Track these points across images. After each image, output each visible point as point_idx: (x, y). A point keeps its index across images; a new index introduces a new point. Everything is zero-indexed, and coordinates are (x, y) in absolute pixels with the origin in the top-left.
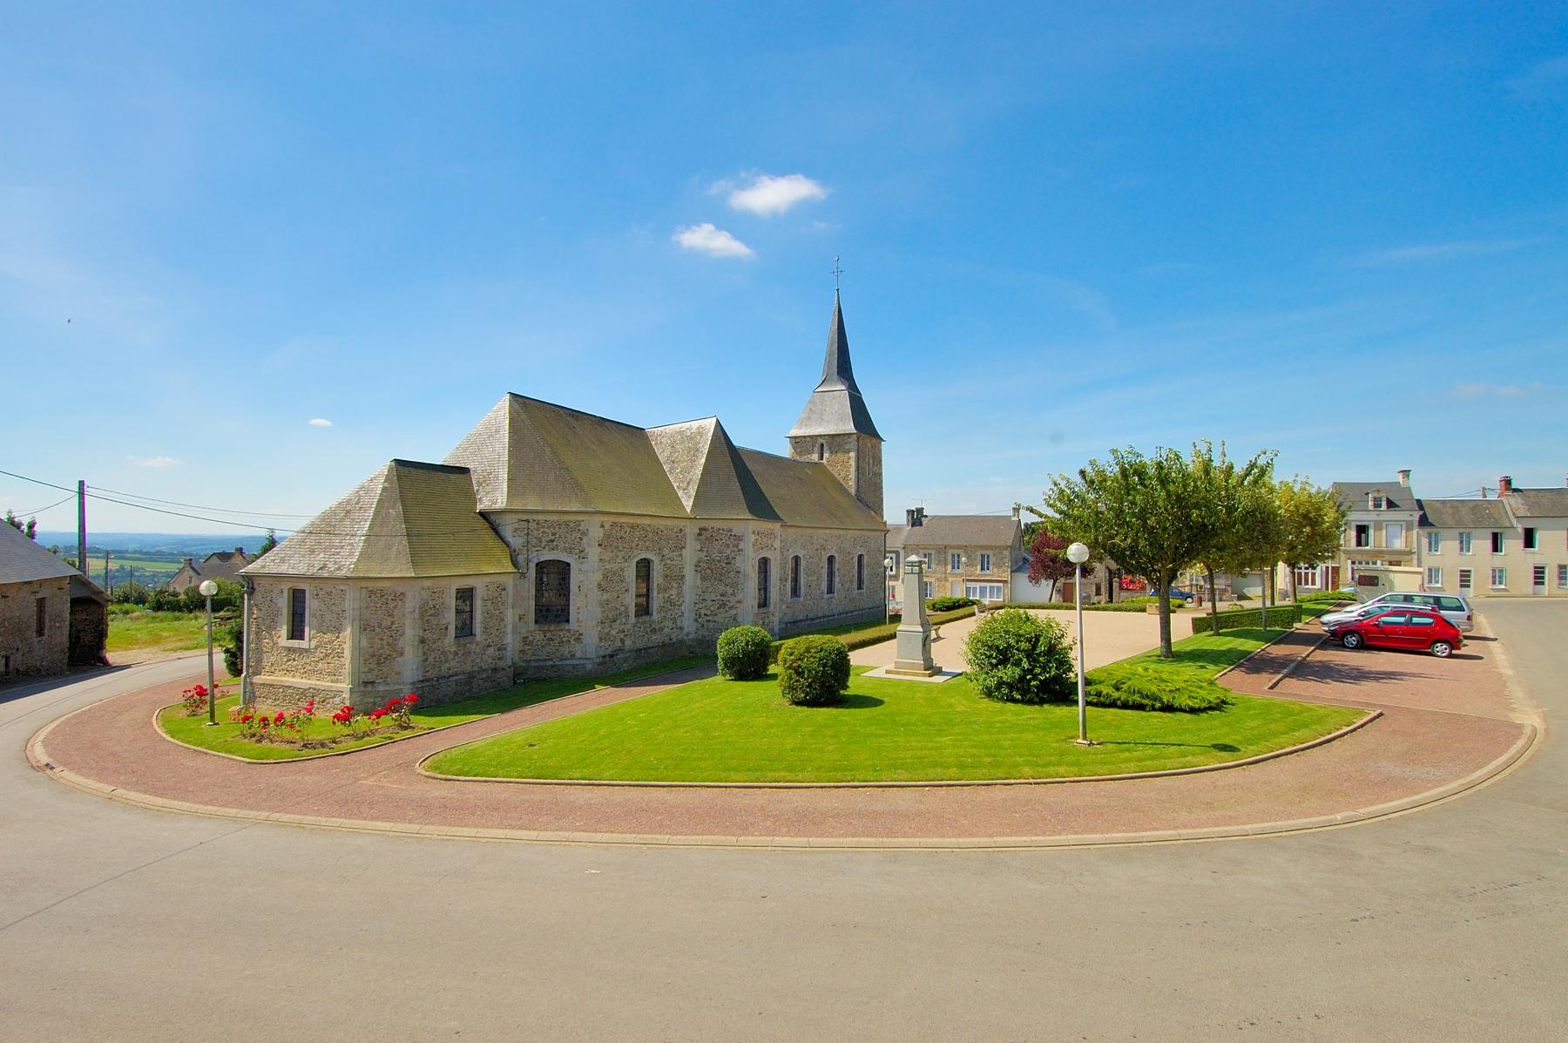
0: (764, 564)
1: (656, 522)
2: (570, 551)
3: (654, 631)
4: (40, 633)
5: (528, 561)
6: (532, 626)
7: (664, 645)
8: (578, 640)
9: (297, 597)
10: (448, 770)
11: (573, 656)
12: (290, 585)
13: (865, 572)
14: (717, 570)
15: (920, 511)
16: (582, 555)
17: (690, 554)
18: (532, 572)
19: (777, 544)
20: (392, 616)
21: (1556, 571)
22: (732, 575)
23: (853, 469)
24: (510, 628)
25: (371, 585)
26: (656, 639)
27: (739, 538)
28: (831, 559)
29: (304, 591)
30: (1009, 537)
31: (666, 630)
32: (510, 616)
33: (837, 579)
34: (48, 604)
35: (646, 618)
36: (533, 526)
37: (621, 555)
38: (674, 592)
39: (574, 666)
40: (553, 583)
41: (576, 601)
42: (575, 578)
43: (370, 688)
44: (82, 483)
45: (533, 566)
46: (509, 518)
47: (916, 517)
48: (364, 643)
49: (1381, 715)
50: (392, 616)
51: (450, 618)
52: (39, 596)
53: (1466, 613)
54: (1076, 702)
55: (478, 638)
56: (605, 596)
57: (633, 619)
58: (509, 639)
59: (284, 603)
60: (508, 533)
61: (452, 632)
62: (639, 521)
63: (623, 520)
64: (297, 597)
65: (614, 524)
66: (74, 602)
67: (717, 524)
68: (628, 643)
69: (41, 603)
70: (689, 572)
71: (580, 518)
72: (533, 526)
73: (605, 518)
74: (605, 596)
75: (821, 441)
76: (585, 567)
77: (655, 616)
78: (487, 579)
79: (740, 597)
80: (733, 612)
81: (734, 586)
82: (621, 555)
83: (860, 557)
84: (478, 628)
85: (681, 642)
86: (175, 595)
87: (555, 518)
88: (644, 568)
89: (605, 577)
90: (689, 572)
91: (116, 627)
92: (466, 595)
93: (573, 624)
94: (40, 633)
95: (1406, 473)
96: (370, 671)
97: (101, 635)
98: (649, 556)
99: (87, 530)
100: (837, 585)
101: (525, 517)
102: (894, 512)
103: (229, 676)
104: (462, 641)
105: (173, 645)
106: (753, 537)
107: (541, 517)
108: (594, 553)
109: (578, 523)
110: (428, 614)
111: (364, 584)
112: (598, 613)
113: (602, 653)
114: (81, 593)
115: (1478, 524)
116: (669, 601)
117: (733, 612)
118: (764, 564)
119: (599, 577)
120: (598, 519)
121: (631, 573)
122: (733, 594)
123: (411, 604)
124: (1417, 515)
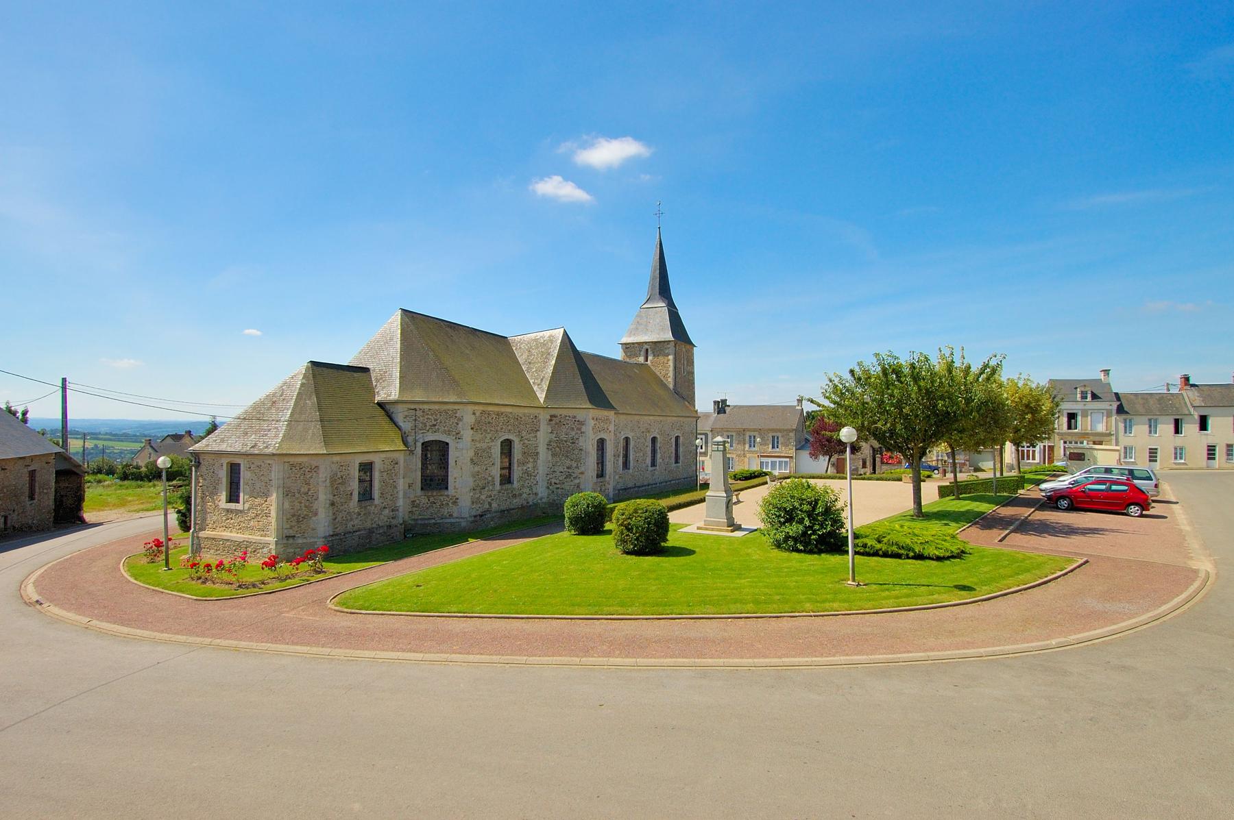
0: (601, 443)
1: (515, 410)
2: (448, 433)
3: (515, 496)
4: (32, 497)
5: (416, 441)
6: (419, 492)
7: (523, 507)
8: (455, 503)
9: (234, 470)
10: (351, 605)
11: (451, 515)
12: (228, 460)
13: (681, 449)
14: (565, 448)
15: (724, 401)
16: (458, 437)
17: (543, 435)
18: (419, 450)
19: (612, 428)
20: (308, 484)
21: (1224, 449)
22: (576, 452)
23: (671, 369)
24: (401, 495)
25: (292, 460)
26: (517, 502)
27: (582, 423)
28: (654, 440)
29: (239, 465)
30: (794, 422)
31: (525, 496)
32: (402, 484)
33: (659, 456)
34: (37, 475)
35: (509, 486)
36: (419, 413)
37: (489, 436)
38: (530, 465)
39: (452, 524)
40: (435, 458)
41: (453, 473)
42: (452, 454)
43: (291, 541)
44: (64, 380)
45: (419, 445)
46: (400, 407)
47: (721, 407)
48: (287, 505)
49: (1087, 562)
50: (308, 484)
51: (355, 486)
52: (30, 469)
53: (1154, 482)
54: (847, 552)
55: (376, 502)
56: (477, 469)
57: (498, 487)
58: (400, 502)
59: (223, 474)
60: (399, 419)
61: (356, 497)
62: (503, 409)
63: (490, 408)
64: (234, 470)
65: (483, 412)
66: (58, 473)
67: (564, 412)
68: (494, 505)
69: (32, 474)
70: (542, 449)
71: (456, 407)
72: (419, 413)
73: (476, 407)
74: (477, 469)
75: (646, 346)
76: (460, 446)
77: (516, 484)
78: (383, 455)
79: (582, 469)
80: (577, 481)
81: (578, 460)
82: (489, 436)
83: (677, 438)
84: (376, 494)
85: (536, 505)
86: (138, 467)
87: (437, 407)
88: (507, 446)
89: (476, 454)
90: (542, 449)
91: (91, 493)
92: (367, 468)
93: (451, 491)
94: (32, 497)
95: (1106, 372)
96: (291, 527)
97: (80, 499)
98: (511, 437)
99: (69, 417)
100: (659, 460)
101: (413, 407)
102: (704, 403)
103: (181, 532)
104: (364, 504)
105: (136, 508)
106: (592, 422)
107: (426, 407)
108: (467, 435)
109: (455, 411)
110: (337, 482)
111: (286, 459)
112: (471, 482)
113: (474, 513)
114: (64, 466)
115: (1164, 412)
116: (526, 472)
117: (577, 481)
118: (601, 443)
119: (471, 453)
120: (470, 408)
121: (496, 450)
122: (577, 467)
123: (324, 474)
124: (1115, 405)
